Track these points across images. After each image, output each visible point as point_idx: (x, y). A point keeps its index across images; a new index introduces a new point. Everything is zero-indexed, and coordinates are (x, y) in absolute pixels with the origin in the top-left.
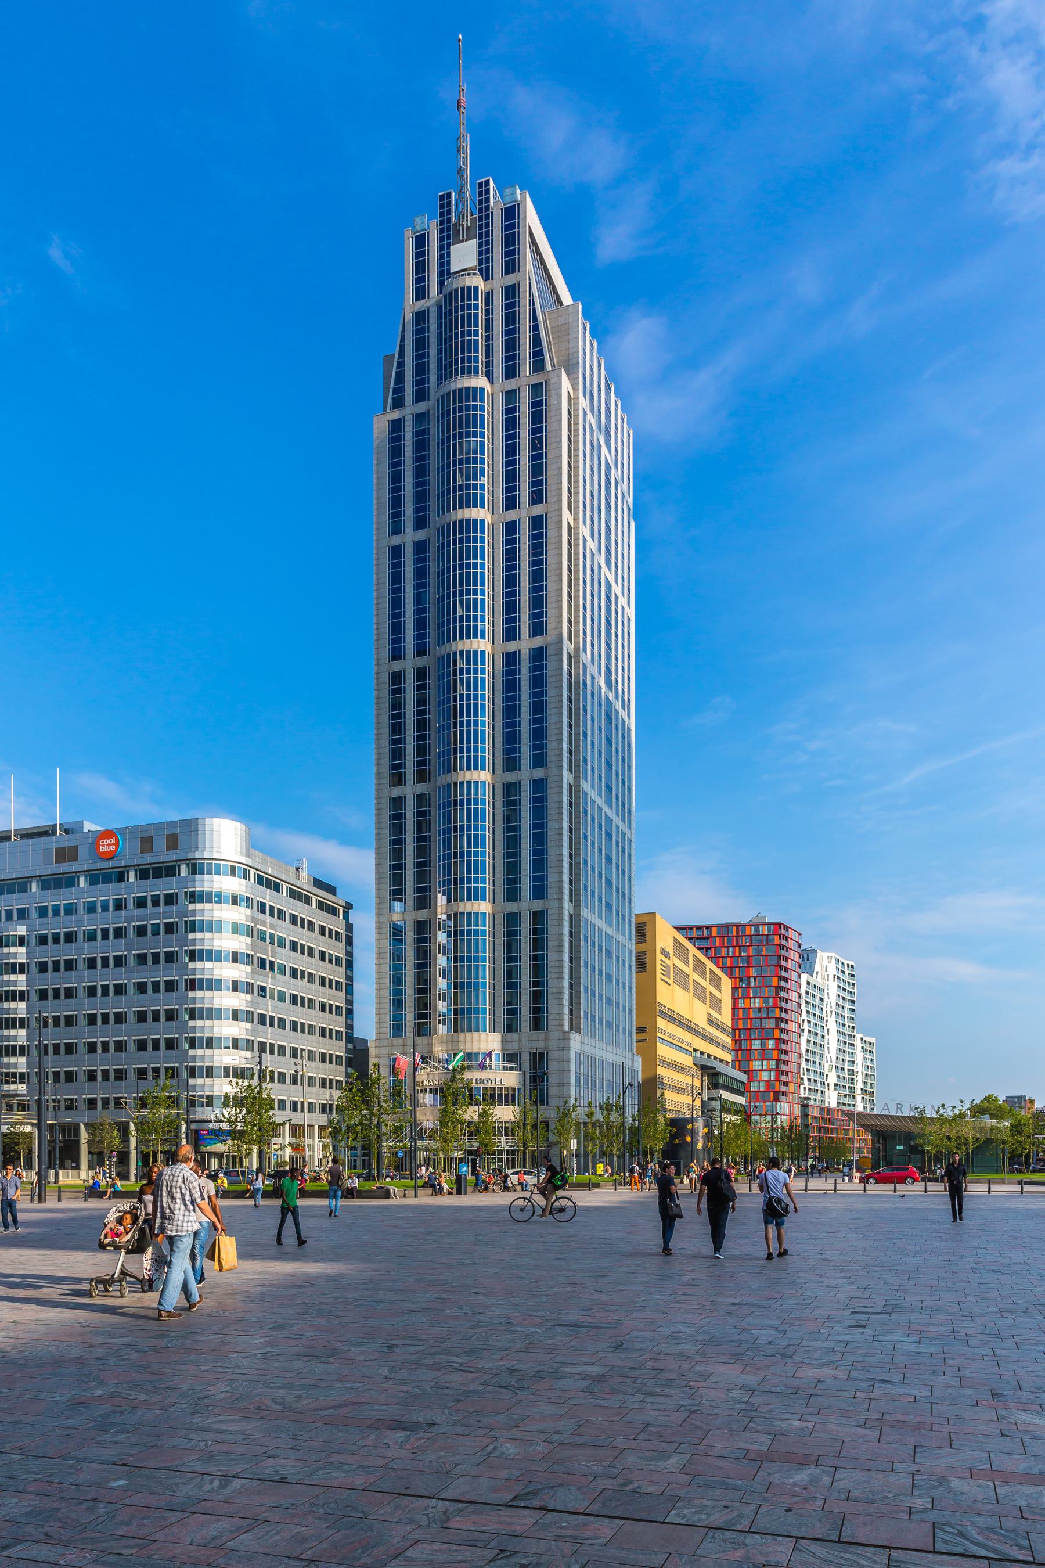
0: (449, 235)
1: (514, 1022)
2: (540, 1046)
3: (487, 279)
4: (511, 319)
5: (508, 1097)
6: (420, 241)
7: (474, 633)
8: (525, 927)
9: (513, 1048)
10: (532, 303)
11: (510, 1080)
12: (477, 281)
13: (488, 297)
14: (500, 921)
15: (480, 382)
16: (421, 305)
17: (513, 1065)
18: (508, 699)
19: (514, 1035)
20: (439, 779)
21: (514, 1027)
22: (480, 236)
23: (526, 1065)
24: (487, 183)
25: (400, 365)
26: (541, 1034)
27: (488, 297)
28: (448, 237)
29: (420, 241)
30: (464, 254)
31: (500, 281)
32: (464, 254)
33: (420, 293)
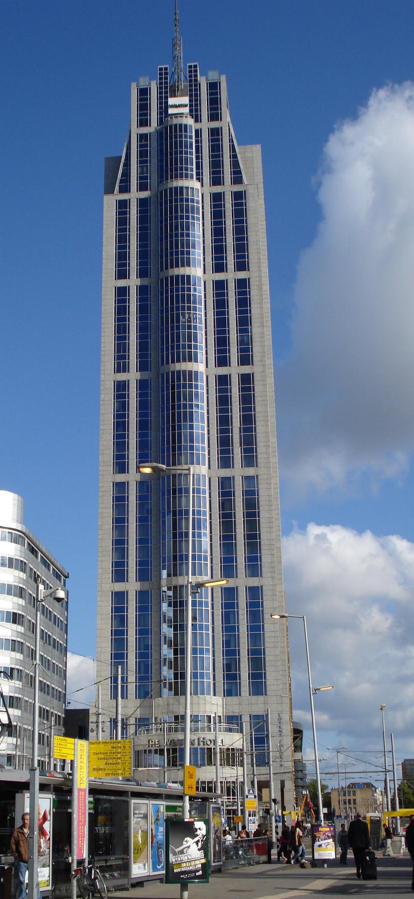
0: (168, 90)
1: (234, 688)
2: (258, 710)
3: (196, 121)
4: (216, 148)
5: (231, 757)
6: (144, 93)
7: (192, 358)
8: (242, 600)
9: (235, 710)
10: (231, 141)
11: (235, 740)
12: (190, 121)
13: (198, 133)
14: (210, 287)
15: (197, 185)
16: (144, 130)
17: (235, 727)
18: (222, 431)
19: (233, 699)
20: (171, 365)
21: (234, 691)
22: (191, 96)
23: (246, 727)
24: (195, 66)
25: (127, 164)
26: (261, 698)
27: (198, 133)
28: (166, 93)
29: (144, 93)
30: (179, 103)
31: (206, 125)
32: (179, 103)
33: (144, 122)
